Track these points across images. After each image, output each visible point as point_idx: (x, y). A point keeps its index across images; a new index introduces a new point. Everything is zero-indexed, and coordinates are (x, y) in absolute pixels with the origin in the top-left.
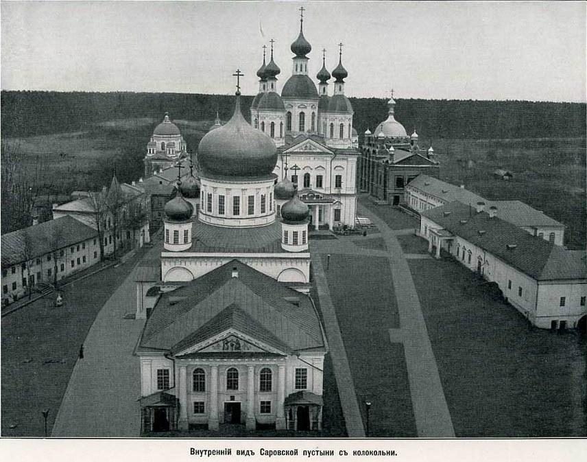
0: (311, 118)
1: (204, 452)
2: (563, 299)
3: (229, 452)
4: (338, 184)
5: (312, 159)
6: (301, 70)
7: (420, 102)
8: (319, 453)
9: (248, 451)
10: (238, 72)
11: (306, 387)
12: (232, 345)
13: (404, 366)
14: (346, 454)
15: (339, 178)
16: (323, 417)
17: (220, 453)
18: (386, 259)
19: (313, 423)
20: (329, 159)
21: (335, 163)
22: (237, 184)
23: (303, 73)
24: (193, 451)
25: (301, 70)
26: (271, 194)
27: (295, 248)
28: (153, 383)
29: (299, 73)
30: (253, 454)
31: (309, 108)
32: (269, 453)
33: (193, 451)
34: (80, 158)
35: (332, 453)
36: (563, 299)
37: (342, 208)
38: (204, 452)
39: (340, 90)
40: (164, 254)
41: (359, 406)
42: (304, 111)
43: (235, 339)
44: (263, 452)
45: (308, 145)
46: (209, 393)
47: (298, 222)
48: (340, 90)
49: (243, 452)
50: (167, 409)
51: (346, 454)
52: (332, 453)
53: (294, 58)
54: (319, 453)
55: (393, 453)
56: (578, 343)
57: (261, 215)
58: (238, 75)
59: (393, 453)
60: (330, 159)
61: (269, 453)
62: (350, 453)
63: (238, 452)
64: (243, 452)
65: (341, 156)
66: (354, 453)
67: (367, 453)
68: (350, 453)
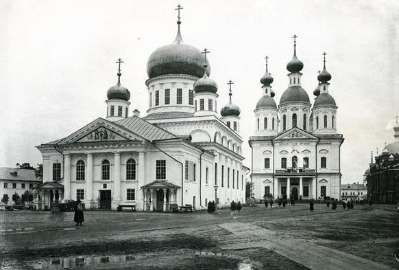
0: (303, 118)
4: (324, 164)
5: (299, 144)
6: (295, 83)
10: (179, 6)
11: (165, 178)
12: (101, 135)
15: (324, 160)
20: (314, 144)
21: (319, 148)
23: (296, 84)
25: (295, 83)
26: (318, 244)
27: (202, 113)
29: (293, 85)
31: (300, 110)
37: (327, 185)
39: (324, 89)
42: (296, 112)
43: (104, 129)
45: (295, 133)
48: (324, 89)
53: (288, 75)
57: (188, 105)
58: (179, 9)
60: (315, 144)
65: (325, 141)
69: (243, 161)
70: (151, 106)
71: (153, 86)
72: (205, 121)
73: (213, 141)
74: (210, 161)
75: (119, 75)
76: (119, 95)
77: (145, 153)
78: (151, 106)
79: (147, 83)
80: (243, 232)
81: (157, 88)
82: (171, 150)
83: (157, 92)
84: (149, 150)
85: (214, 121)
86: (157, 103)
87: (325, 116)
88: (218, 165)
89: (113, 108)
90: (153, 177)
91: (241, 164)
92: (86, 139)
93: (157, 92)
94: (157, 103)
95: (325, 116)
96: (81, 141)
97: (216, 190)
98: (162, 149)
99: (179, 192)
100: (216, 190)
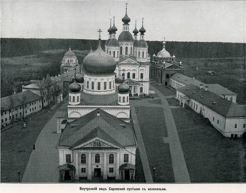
0: (130, 49)
1: (85, 189)
2: (236, 125)
3: (96, 189)
4: (142, 77)
5: (131, 66)
6: (126, 29)
7: (176, 43)
8: (134, 189)
9: (104, 188)
10: (100, 30)
11: (128, 162)
12: (97, 144)
13: (169, 153)
14: (145, 190)
15: (142, 74)
16: (135, 174)
17: (92, 189)
18: (162, 108)
19: (131, 177)
20: (138, 66)
21: (141, 68)
22: (99, 77)
23: (127, 31)
24: (81, 189)
25: (126, 29)
26: (114, 81)
27: (124, 104)
28: (64, 160)
29: (125, 30)
30: (106, 189)
31: (130, 45)
32: (113, 189)
33: (81, 189)
34: (34, 66)
35: (139, 189)
36: (236, 125)
37: (143, 87)
38: (85, 189)
40: (69, 106)
41: (151, 170)
42: (127, 46)
43: (98, 142)
44: (110, 189)
45: (129, 61)
46: (88, 164)
47: (125, 93)
49: (102, 189)
50: (70, 171)
51: (145, 190)
52: (139, 189)
53: (123, 24)
54: (134, 189)
55: (165, 189)
56: (242, 143)
57: (109, 90)
58: (100, 31)
59: (165, 189)
60: (138, 66)
61: (113, 189)
62: (147, 189)
63: (100, 189)
64: (102, 189)
65: (143, 65)
66: (149, 189)
67: (154, 189)
68: (147, 189)
80: (34, 92)
87: (139, 52)
95: (139, 52)
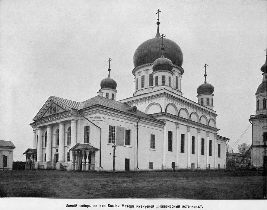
24: (68, 206)
35: (76, 206)
69: (218, 132)
70: (137, 89)
71: (139, 72)
72: (155, 96)
73: (164, 111)
74: (161, 129)
75: (109, 70)
76: (109, 84)
77: (77, 121)
78: (137, 89)
79: (134, 72)
81: (143, 73)
82: (92, 116)
83: (143, 77)
84: (79, 118)
85: (164, 94)
86: (143, 85)
88: (196, 139)
89: (202, 100)
90: (82, 141)
91: (215, 134)
92: (46, 115)
93: (143, 77)
94: (143, 85)
96: (43, 117)
97: (114, 150)
98: (87, 117)
99: (97, 154)
100: (114, 150)
